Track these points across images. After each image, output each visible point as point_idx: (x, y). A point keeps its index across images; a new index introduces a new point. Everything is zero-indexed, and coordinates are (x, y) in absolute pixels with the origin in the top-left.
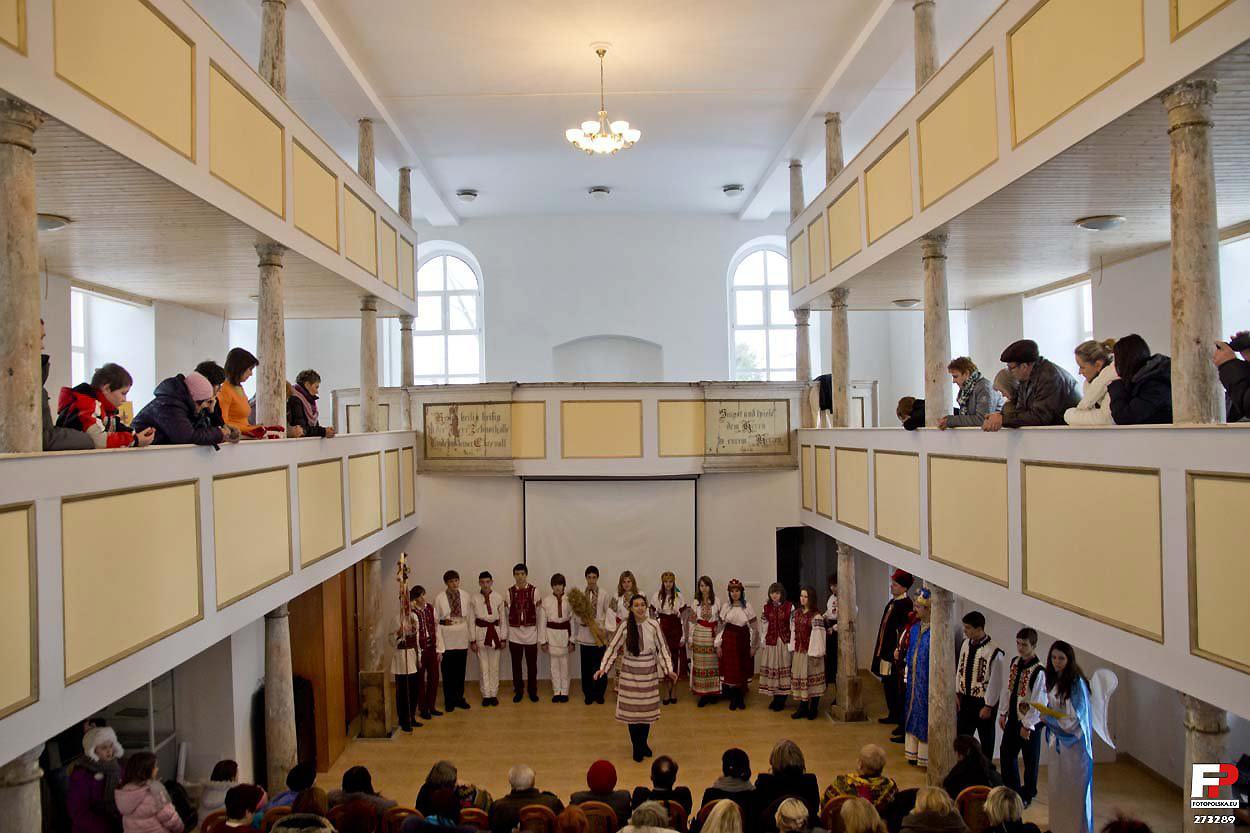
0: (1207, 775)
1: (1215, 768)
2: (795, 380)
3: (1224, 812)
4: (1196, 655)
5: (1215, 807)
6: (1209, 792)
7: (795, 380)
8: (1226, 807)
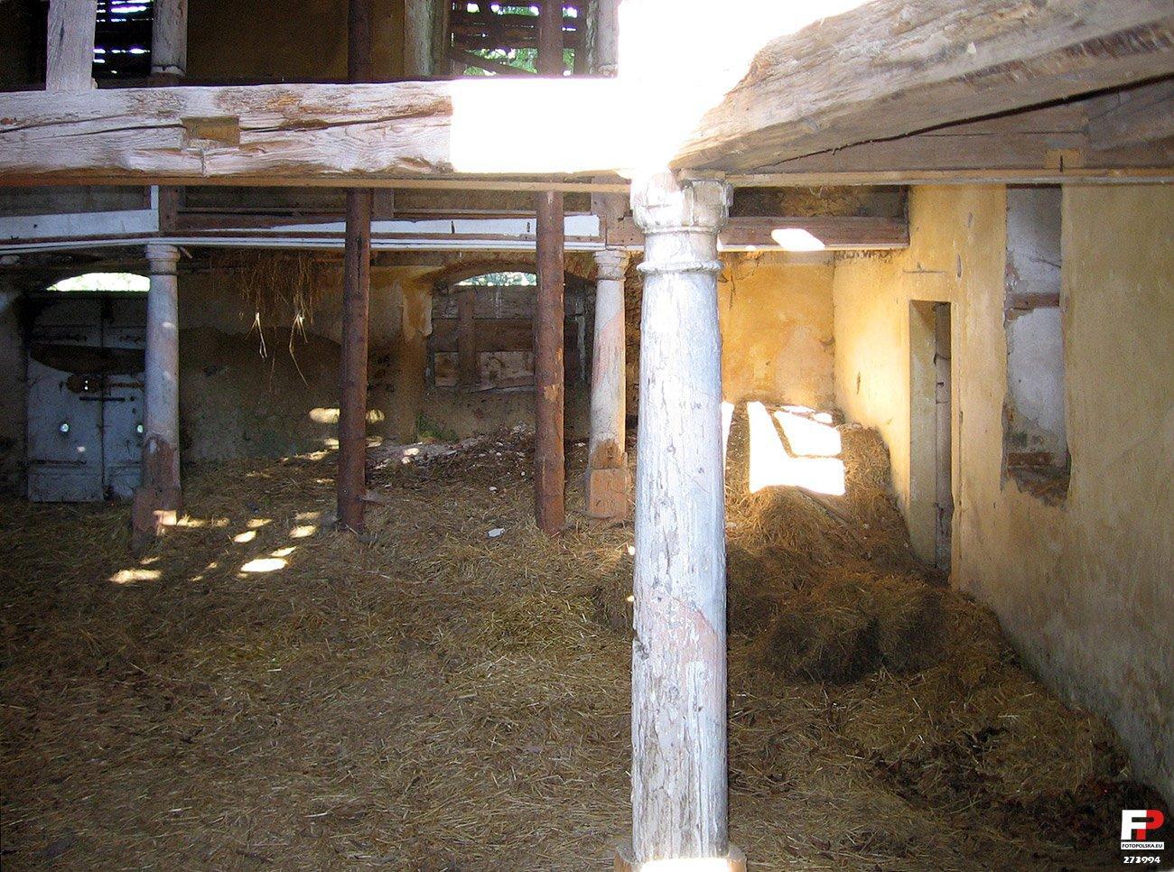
0: (1135, 820)
1: (1142, 813)
2: (1124, 811)
4: (632, 422)
7: (1124, 811)
8: (1153, 848)
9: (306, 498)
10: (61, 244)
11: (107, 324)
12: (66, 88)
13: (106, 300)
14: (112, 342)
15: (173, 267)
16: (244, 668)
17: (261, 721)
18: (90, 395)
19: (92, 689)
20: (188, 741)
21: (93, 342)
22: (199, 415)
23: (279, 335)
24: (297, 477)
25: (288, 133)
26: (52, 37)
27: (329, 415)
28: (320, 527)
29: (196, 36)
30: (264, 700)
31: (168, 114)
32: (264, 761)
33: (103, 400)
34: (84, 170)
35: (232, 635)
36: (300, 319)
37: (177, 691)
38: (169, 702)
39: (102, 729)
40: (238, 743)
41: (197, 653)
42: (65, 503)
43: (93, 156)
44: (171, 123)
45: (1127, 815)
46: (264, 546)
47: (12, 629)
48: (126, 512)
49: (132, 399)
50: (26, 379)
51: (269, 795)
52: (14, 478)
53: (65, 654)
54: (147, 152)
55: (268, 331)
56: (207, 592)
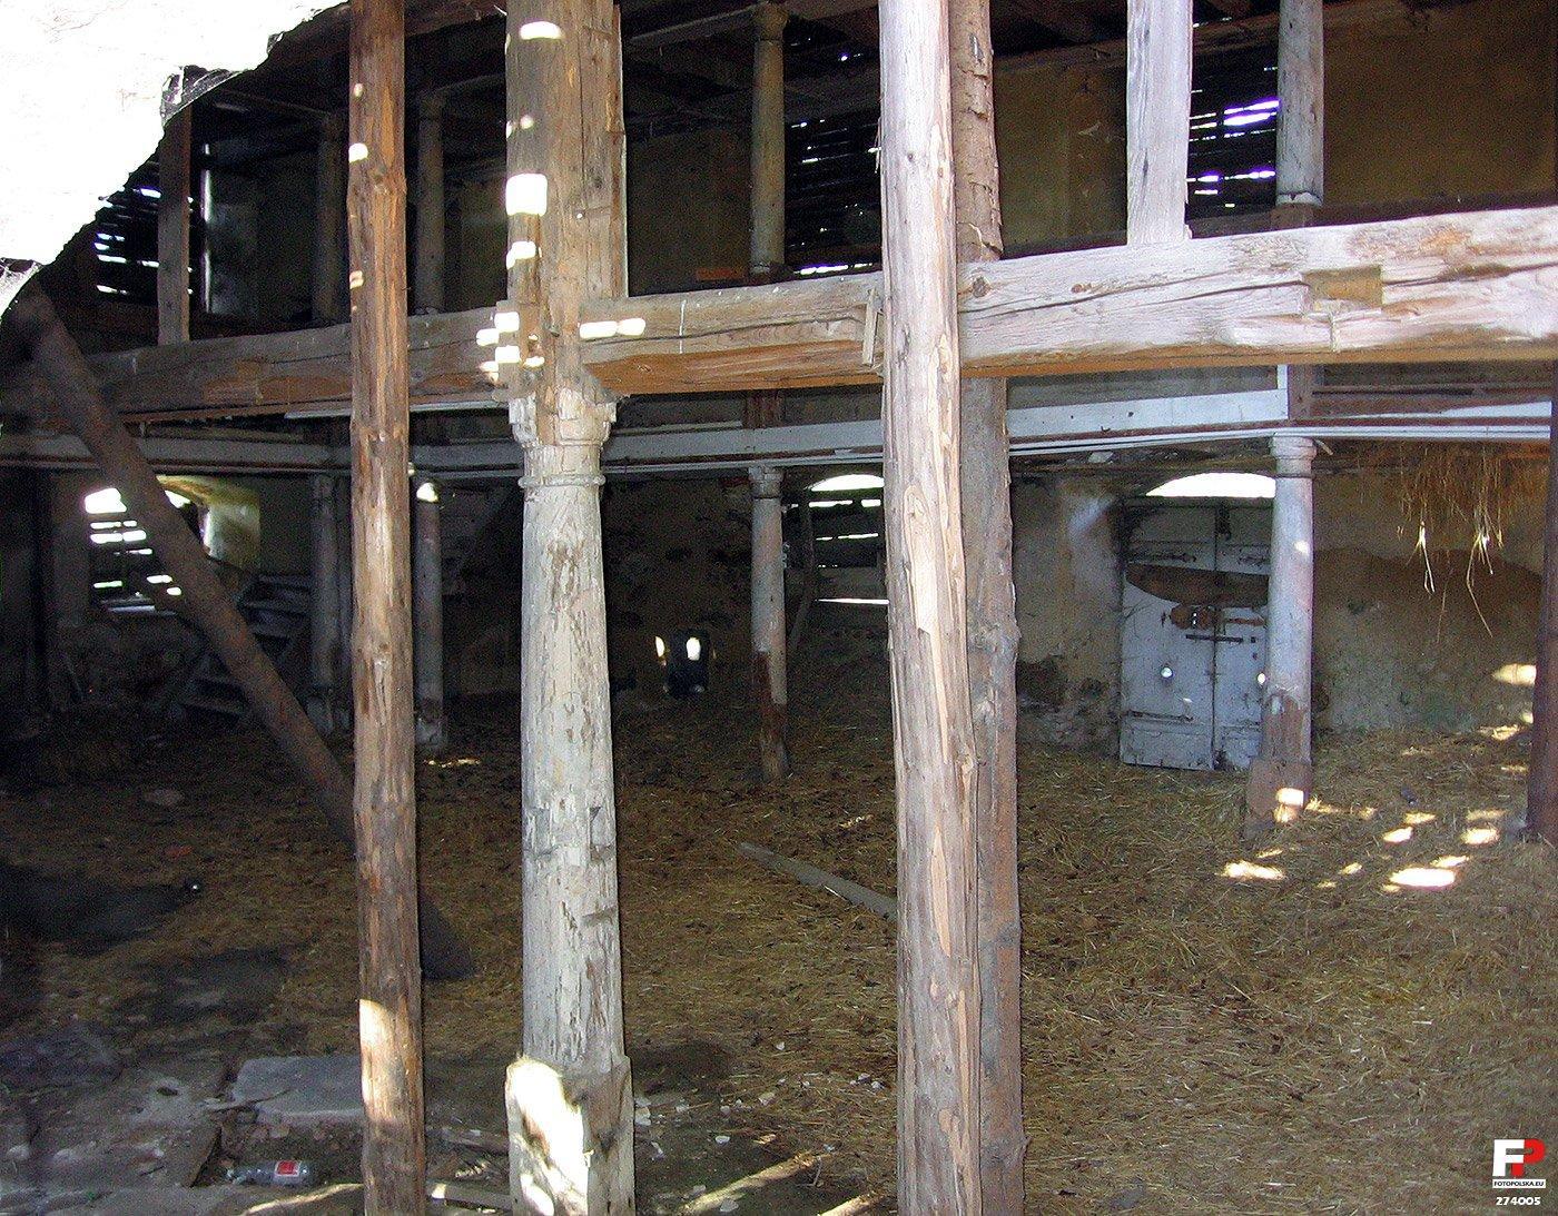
0: (1509, 1152)
1: (1520, 1144)
3: (1534, 1193)
5: (1519, 1187)
6: (1513, 1170)
8: (1531, 1187)
9: (1484, 790)
10: (1161, 437)
11: (1223, 543)
12: (1153, 240)
13: (1222, 509)
14: (1229, 565)
15: (1305, 467)
16: (1380, 1014)
17: (1398, 1088)
18: (1199, 633)
19: (1181, 1011)
20: (1298, 1097)
21: (1205, 563)
22: (1339, 666)
23: (1452, 563)
24: (1472, 760)
25: (1450, 285)
26: (1133, 174)
27: (1527, 674)
28: (1502, 833)
29: (1335, 148)
30: (1404, 1060)
31: (1283, 268)
32: (1398, 1143)
33: (1216, 640)
34: (1175, 348)
35: (1366, 965)
36: (1482, 540)
37: (1289, 1030)
38: (1278, 1043)
39: (1191, 1064)
40: (1364, 1111)
41: (1320, 985)
42: (1163, 768)
43: (1189, 330)
44: (1286, 281)
45: (1501, 1146)
46: (1423, 851)
47: (1090, 921)
48: (1239, 787)
49: (1253, 640)
50: (1119, 608)
51: (1400, 1190)
52: (1104, 731)
53: (1149, 961)
54: (1256, 321)
55: (1438, 557)
56: (1337, 905)
